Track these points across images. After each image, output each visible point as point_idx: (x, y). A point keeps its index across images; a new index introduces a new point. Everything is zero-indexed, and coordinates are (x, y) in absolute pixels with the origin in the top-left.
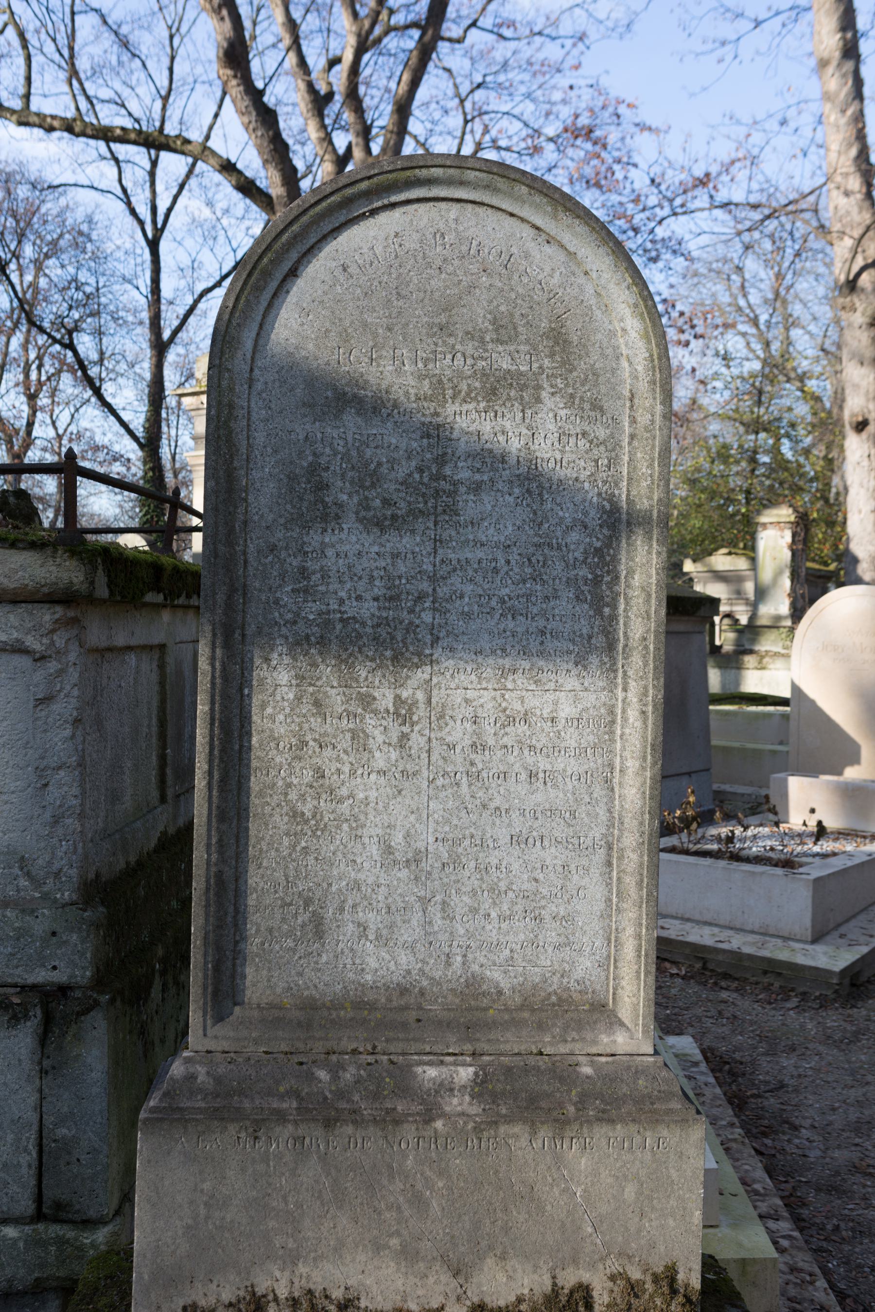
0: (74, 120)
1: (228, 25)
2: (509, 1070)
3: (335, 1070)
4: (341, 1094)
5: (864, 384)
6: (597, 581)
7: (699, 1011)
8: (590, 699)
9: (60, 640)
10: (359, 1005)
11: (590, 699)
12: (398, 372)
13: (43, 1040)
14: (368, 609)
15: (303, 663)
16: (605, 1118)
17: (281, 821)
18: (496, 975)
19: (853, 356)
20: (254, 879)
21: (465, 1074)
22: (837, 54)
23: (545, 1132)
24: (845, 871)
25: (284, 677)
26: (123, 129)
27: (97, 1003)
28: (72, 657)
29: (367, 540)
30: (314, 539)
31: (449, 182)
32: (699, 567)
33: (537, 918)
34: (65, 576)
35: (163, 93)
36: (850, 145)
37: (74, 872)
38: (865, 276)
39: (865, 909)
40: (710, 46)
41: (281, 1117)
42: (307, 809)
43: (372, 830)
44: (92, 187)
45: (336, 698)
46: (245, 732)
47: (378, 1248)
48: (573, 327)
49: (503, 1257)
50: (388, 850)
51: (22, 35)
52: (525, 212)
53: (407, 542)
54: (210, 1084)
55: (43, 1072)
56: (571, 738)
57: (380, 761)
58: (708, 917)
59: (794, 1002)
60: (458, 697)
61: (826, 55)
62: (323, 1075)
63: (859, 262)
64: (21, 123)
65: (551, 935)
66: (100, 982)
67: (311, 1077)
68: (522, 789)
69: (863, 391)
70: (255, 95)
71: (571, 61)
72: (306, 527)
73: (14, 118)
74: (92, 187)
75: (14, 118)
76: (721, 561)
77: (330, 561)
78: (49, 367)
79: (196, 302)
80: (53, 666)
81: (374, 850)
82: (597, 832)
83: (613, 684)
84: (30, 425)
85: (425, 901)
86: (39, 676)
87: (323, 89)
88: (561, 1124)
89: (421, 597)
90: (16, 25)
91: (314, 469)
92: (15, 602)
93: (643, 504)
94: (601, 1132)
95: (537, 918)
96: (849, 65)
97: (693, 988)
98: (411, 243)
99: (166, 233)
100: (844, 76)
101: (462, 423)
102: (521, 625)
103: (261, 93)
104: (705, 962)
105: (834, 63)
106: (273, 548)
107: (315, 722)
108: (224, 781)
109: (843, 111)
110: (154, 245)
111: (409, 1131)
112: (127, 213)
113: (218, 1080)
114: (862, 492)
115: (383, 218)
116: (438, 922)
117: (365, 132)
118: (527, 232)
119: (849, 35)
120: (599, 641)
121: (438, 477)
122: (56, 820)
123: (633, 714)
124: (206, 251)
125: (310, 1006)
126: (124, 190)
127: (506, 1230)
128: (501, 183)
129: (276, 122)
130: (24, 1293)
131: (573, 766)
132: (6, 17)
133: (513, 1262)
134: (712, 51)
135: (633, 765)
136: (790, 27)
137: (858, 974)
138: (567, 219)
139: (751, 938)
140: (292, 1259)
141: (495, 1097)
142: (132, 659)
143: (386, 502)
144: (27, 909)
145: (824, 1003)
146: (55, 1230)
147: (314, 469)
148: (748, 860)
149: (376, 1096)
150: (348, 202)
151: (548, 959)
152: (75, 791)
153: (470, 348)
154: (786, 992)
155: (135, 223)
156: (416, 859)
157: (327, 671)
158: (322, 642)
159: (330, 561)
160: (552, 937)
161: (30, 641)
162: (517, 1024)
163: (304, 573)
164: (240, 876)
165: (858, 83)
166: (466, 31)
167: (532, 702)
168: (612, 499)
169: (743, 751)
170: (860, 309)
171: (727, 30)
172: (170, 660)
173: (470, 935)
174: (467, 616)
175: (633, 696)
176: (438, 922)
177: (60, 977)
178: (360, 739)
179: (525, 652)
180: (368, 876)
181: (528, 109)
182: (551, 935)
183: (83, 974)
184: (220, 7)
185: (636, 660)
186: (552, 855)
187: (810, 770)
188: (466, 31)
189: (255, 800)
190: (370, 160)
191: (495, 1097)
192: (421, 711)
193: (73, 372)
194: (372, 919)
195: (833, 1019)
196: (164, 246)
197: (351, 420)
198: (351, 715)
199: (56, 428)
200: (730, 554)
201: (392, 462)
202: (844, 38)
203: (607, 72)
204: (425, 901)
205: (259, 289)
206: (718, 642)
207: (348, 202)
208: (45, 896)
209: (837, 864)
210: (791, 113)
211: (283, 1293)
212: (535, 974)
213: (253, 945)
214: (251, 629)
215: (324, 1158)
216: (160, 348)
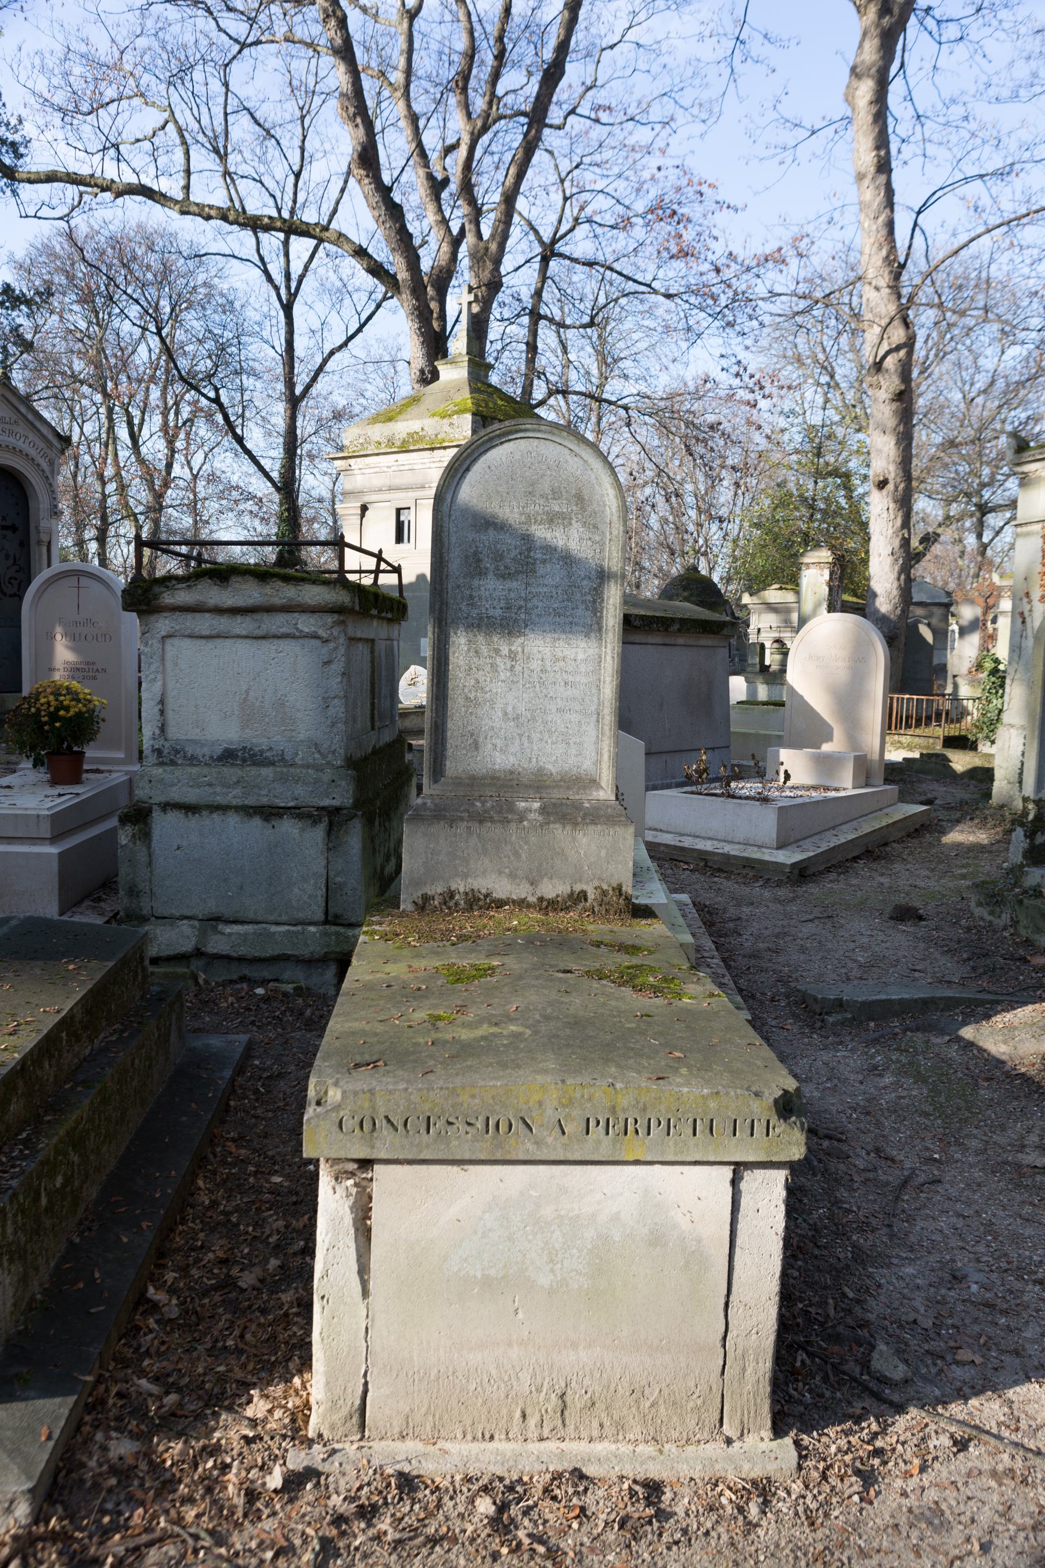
0: (229, 209)
1: (361, 131)
2: (554, 805)
3: (483, 803)
4: (486, 811)
5: (886, 449)
6: (594, 602)
7: (698, 886)
8: (591, 651)
9: (335, 632)
10: (493, 778)
11: (591, 651)
12: (512, 512)
13: (329, 833)
14: (498, 612)
15: (471, 635)
16: (594, 822)
17: (461, 701)
18: (550, 767)
19: (878, 426)
20: (450, 725)
21: (536, 805)
22: (872, 169)
23: (568, 828)
24: (804, 804)
25: (463, 640)
26: (270, 218)
27: (356, 815)
28: (342, 640)
29: (498, 583)
30: (476, 582)
31: (534, 430)
32: (755, 600)
33: (568, 743)
34: (340, 598)
35: (296, 168)
36: (880, 248)
37: (342, 751)
38: (889, 359)
39: (820, 833)
40: (772, 151)
41: (462, 819)
42: (472, 696)
43: (499, 706)
44: (234, 256)
45: (484, 650)
46: (447, 664)
47: (500, 873)
48: (586, 493)
49: (551, 878)
50: (506, 714)
51: (180, 131)
52: (566, 443)
53: (514, 584)
54: (432, 807)
55: (329, 849)
56: (583, 668)
57: (502, 677)
58: (711, 835)
59: (761, 883)
60: (535, 650)
61: (863, 170)
62: (478, 804)
63: (885, 347)
64: (183, 213)
65: (573, 751)
66: (357, 804)
67: (473, 805)
68: (562, 689)
69: (884, 455)
70: (384, 191)
71: (660, 143)
72: (472, 577)
73: (177, 207)
74: (234, 256)
75: (177, 207)
76: (773, 595)
77: (483, 592)
78: (186, 411)
79: (325, 361)
80: (332, 645)
81: (500, 714)
82: (593, 708)
83: (600, 645)
84: (169, 466)
85: (521, 736)
86: (325, 650)
87: (439, 176)
88: (575, 824)
89: (520, 608)
90: (176, 122)
91: (476, 553)
92: (313, 612)
93: (614, 569)
94: (592, 828)
95: (568, 743)
96: (882, 179)
97: (697, 875)
98: (517, 456)
99: (299, 298)
100: (877, 188)
101: (538, 534)
102: (562, 620)
103: (390, 189)
104: (706, 861)
105: (870, 177)
106: (458, 587)
107: (475, 660)
108: (438, 683)
109: (876, 218)
110: (288, 309)
111: (513, 825)
112: (264, 278)
113: (436, 805)
114: (882, 538)
115: (506, 445)
116: (526, 744)
117: (477, 213)
118: (567, 451)
119: (883, 153)
120: (595, 627)
121: (528, 557)
122: (333, 725)
123: (609, 658)
124: (334, 313)
125: (473, 778)
126: (262, 259)
127: (552, 867)
128: (556, 431)
129: (402, 216)
130: (318, 961)
131: (584, 680)
132: (166, 115)
133: (555, 881)
134: (774, 156)
135: (608, 679)
136: (842, 133)
137: (805, 868)
138: (583, 446)
139: (737, 847)
140: (465, 876)
141: (548, 814)
142: (360, 645)
143: (506, 567)
144: (319, 769)
145: (779, 884)
146: (334, 928)
147: (476, 553)
148: (740, 798)
149: (500, 812)
150: (491, 439)
151: (572, 760)
152: (343, 709)
153: (542, 502)
154: (756, 878)
155: (270, 288)
156: (517, 718)
157: (481, 638)
158: (479, 626)
159: (483, 592)
160: (574, 751)
161: (321, 632)
162: (558, 787)
163: (471, 597)
164: (444, 723)
165: (890, 192)
166: (565, 118)
167: (567, 652)
168: (601, 566)
169: (757, 735)
170: (884, 387)
171: (789, 137)
172: (376, 648)
173: (539, 750)
174: (539, 616)
175: (609, 651)
176: (526, 744)
177: (336, 803)
178: (494, 666)
179: (564, 632)
180: (497, 725)
181: (621, 187)
182: (573, 751)
183: (348, 802)
184: (355, 115)
185: (610, 635)
186: (574, 717)
187: (795, 744)
188: (565, 118)
189: (450, 692)
190: (482, 244)
191: (548, 814)
192: (520, 656)
193: (209, 417)
194: (499, 743)
195: (783, 892)
196: (297, 309)
197: (491, 532)
198: (491, 657)
199: (191, 469)
200: (781, 589)
201: (509, 550)
202: (878, 156)
203: (693, 152)
204: (521, 736)
205: (453, 477)
206: (767, 662)
207: (491, 439)
208: (328, 763)
209: (799, 801)
210: (836, 215)
211: (462, 890)
212: (566, 767)
213: (449, 752)
214: (449, 621)
215: (479, 836)
216: (294, 402)
